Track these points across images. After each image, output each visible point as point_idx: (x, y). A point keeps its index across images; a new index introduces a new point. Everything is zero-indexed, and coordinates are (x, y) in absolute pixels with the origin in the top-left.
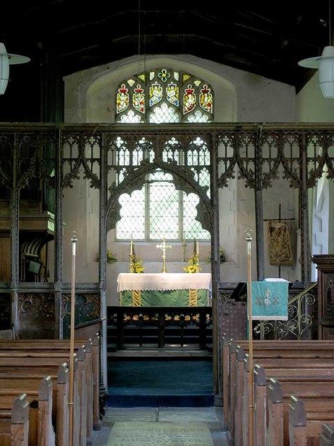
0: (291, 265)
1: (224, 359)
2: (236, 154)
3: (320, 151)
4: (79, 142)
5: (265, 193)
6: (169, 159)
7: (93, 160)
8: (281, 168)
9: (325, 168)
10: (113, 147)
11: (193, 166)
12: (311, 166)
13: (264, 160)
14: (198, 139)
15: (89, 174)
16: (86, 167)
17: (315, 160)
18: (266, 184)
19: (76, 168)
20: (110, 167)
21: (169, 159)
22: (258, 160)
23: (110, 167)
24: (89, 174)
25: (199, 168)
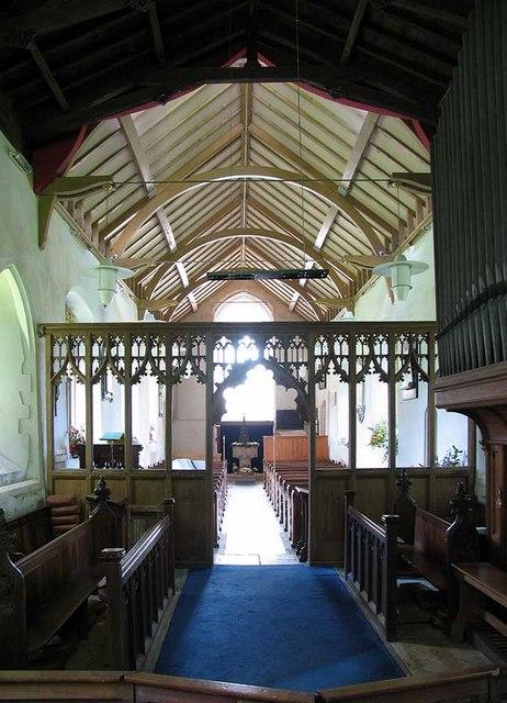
0: (319, 478)
1: (345, 694)
2: (189, 351)
3: (326, 350)
4: (348, 341)
5: (135, 388)
6: (270, 357)
7: (381, 356)
8: (149, 366)
9: (189, 366)
10: (218, 346)
11: (292, 363)
12: (135, 364)
13: (357, 357)
14: (224, 338)
15: (378, 369)
16: (375, 362)
17: (179, 358)
18: (136, 380)
19: (327, 363)
20: (216, 364)
21: (270, 357)
22: (352, 357)
23: (216, 364)
24: (378, 369)
25: (298, 365)
